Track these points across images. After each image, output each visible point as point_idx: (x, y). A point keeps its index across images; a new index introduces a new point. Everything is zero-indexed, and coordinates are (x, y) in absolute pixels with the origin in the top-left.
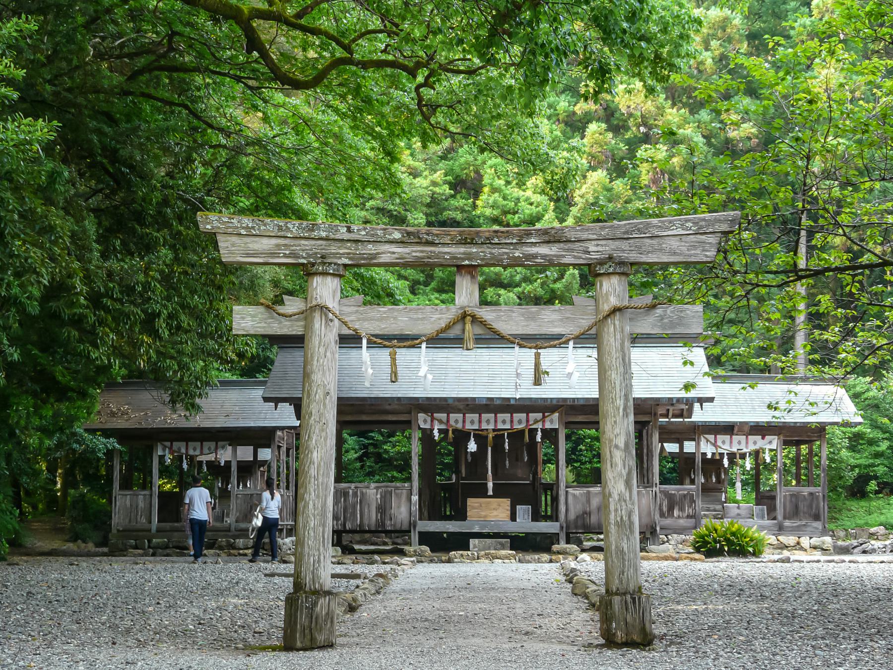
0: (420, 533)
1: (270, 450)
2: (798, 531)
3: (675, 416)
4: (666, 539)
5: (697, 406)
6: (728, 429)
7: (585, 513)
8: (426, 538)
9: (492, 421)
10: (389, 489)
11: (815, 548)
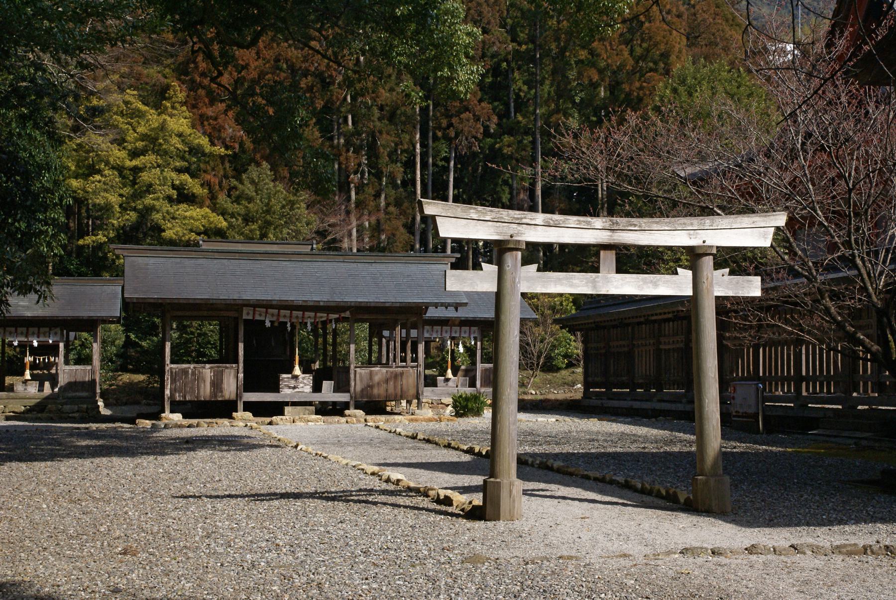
8: (250, 407)
9: (251, 313)
10: (221, 369)
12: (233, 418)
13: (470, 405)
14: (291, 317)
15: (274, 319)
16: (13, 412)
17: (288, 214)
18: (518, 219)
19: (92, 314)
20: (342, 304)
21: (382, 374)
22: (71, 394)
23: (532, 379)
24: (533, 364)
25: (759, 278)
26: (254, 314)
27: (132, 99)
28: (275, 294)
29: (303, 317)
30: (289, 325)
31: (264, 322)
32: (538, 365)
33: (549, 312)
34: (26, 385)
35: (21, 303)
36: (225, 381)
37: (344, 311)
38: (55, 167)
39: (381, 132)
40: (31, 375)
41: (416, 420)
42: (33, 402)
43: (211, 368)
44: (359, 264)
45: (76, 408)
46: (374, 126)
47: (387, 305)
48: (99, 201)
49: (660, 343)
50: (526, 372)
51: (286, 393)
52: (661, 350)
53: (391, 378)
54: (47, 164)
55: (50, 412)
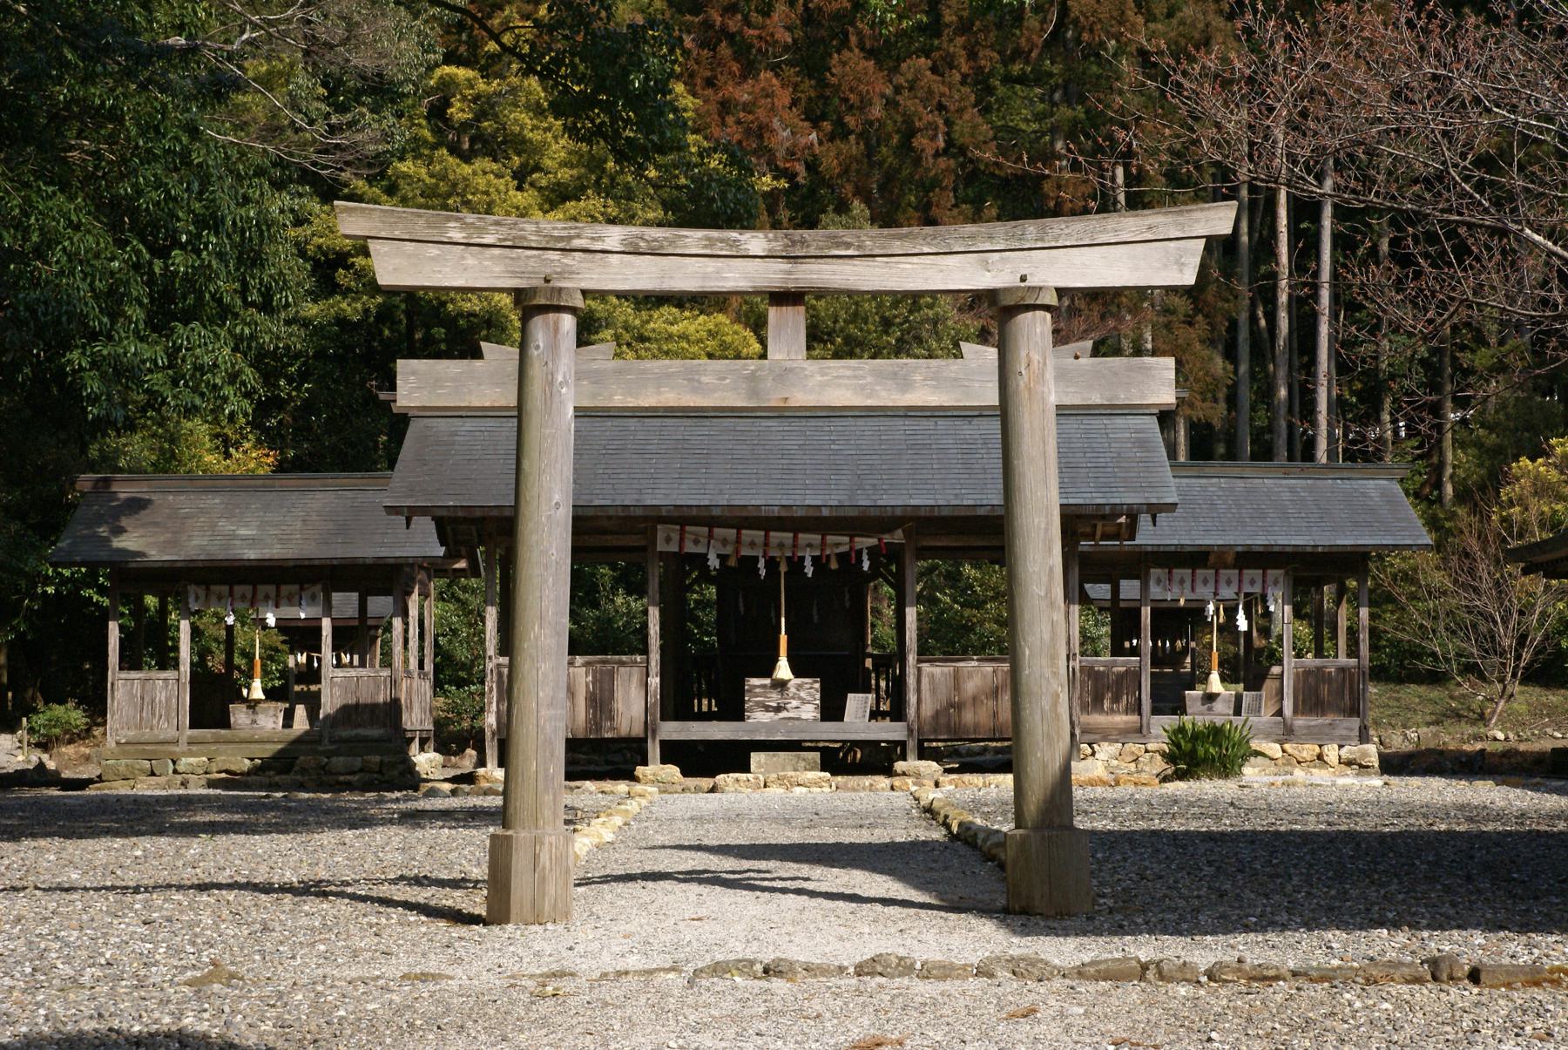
0: (662, 742)
1: (390, 599)
2: (1320, 737)
3: (1105, 537)
4: (1089, 751)
5: (1144, 520)
6: (1195, 559)
7: (951, 705)
8: (674, 753)
9: (675, 537)
10: (609, 667)
11: (1349, 763)
12: (635, 779)
13: (1201, 751)
14: (766, 544)
15: (729, 550)
17: (906, 320)
18: (561, 239)
19: (384, 552)
21: (984, 676)
22: (346, 733)
23: (1502, 703)
25: (1170, 362)
26: (682, 540)
28: (721, 492)
29: (795, 546)
30: (761, 564)
31: (704, 557)
34: (255, 713)
35: (243, 532)
36: (619, 694)
37: (890, 531)
38: (234, 223)
40: (265, 691)
42: (269, 750)
43: (586, 664)
44: (941, 422)
45: (358, 762)
47: (981, 512)
54: (213, 216)
55: (304, 771)
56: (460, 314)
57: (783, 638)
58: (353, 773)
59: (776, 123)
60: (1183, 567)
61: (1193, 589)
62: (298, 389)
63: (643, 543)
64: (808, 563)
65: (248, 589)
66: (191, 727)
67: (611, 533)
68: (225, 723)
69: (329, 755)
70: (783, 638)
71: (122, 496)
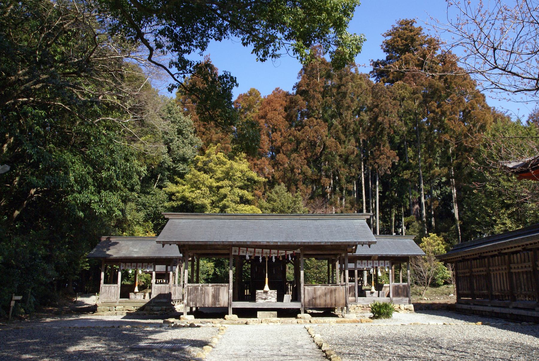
9: (238, 250)
10: (218, 287)
11: (407, 309)
13: (382, 311)
14: (262, 253)
15: (252, 254)
16: (128, 310)
17: (293, 207)
19: (168, 255)
20: (292, 244)
21: (322, 290)
23: (425, 291)
24: (425, 283)
26: (239, 251)
27: (220, 156)
29: (270, 253)
30: (261, 258)
32: (428, 283)
33: (432, 254)
35: (135, 250)
37: (296, 249)
39: (340, 167)
41: (345, 322)
44: (309, 221)
45: (160, 308)
46: (337, 164)
47: (322, 244)
48: (199, 202)
49: (511, 268)
50: (421, 287)
51: (259, 303)
52: (512, 273)
53: (328, 292)
56: (197, 205)
57: (267, 279)
58: (158, 311)
59: (265, 168)
60: (365, 260)
61: (367, 266)
62: (163, 221)
63: (228, 252)
64: (274, 258)
65: (135, 264)
66: (120, 298)
67: (220, 249)
68: (128, 297)
69: (153, 306)
70: (267, 279)
71: (112, 241)
